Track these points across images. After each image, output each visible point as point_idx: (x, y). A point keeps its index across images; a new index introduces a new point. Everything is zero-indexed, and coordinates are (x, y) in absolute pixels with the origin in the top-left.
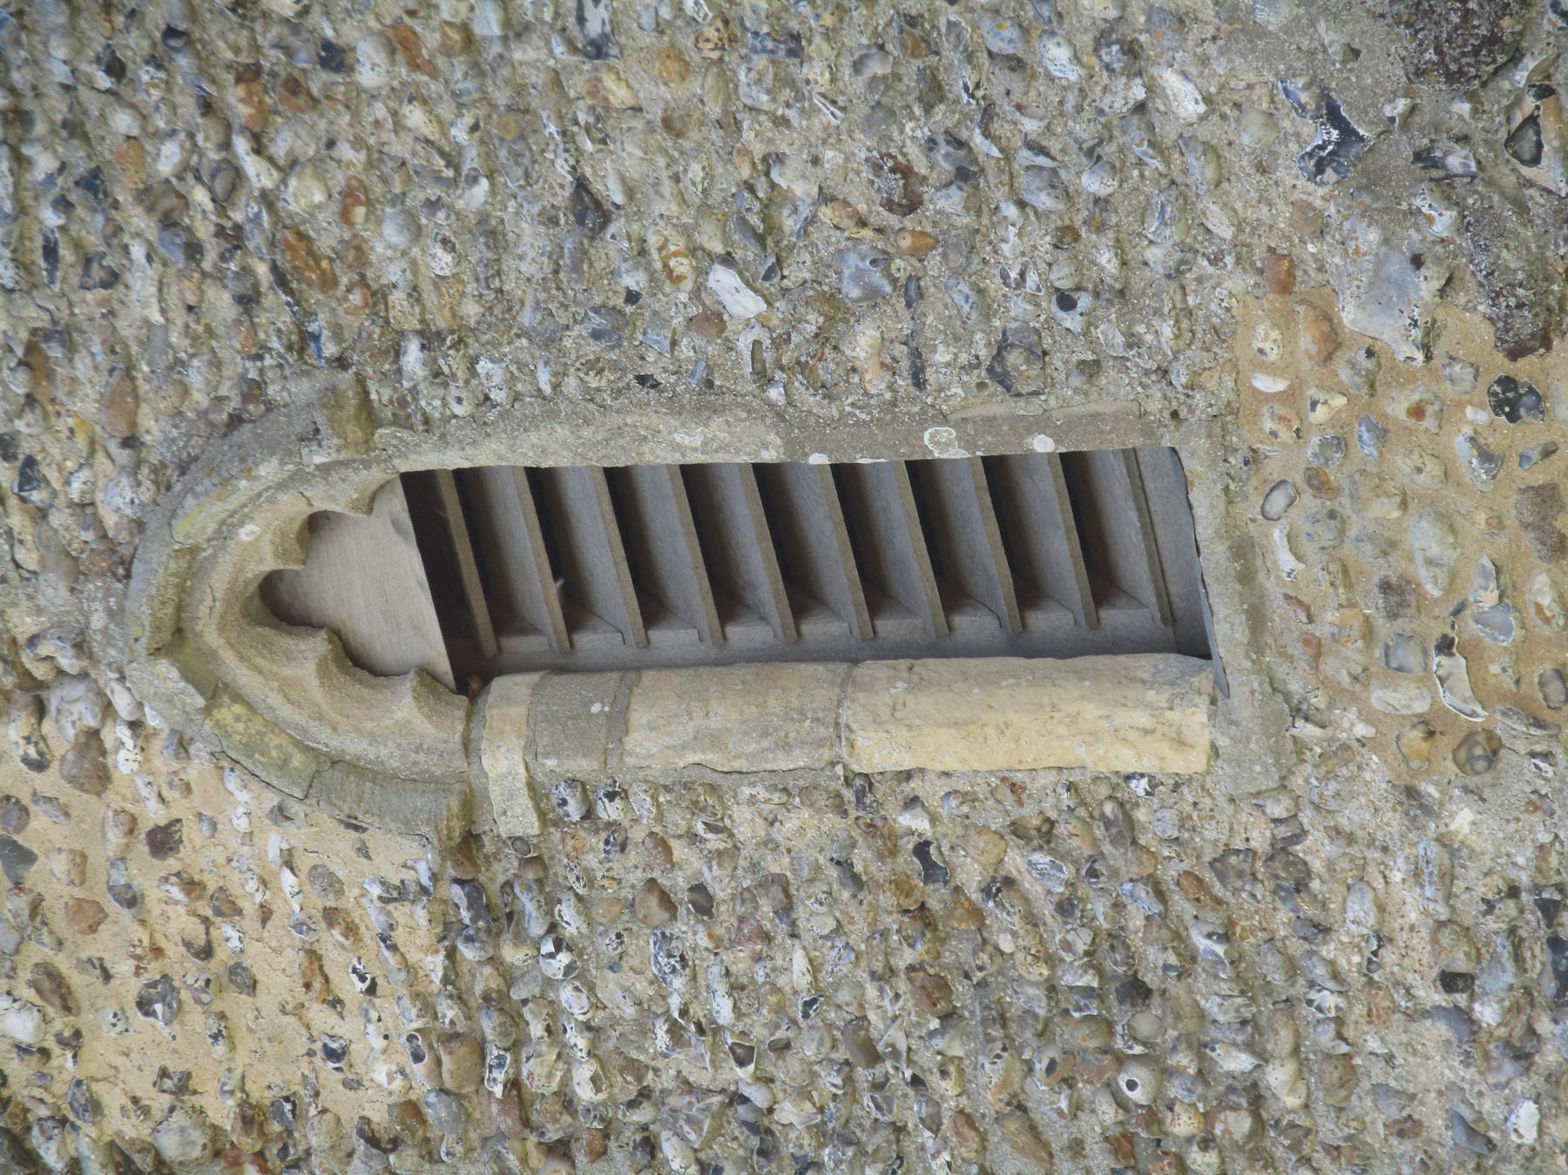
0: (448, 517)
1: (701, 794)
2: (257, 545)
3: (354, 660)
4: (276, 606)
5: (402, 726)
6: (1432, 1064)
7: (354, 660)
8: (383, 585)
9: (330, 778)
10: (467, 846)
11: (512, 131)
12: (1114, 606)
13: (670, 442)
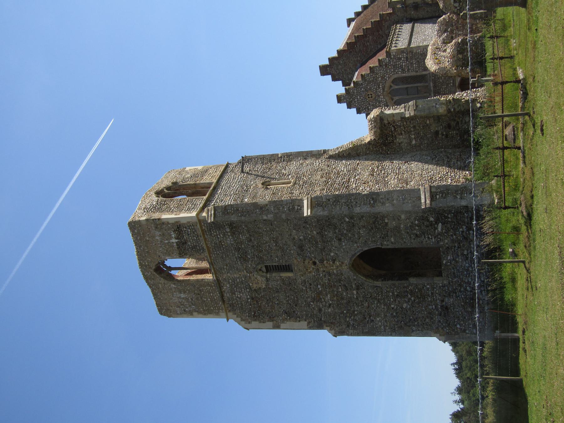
0: (266, 267)
1: (275, 277)
2: (259, 268)
3: (263, 272)
4: (260, 270)
5: (265, 274)
6: (301, 286)
7: (263, 272)
8: (264, 269)
9: (262, 276)
10: (267, 278)
11: (269, 253)
12: (514, 304)
13: (275, 264)
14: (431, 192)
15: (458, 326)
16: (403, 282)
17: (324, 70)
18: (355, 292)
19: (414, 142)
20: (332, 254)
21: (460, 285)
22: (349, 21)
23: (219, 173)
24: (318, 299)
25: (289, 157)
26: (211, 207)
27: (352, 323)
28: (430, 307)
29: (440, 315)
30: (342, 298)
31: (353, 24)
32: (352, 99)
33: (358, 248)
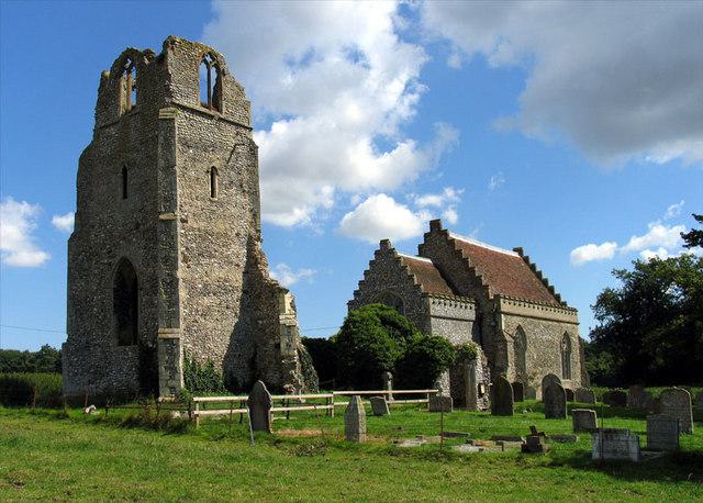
19: (260, 322)
31: (516, 255)
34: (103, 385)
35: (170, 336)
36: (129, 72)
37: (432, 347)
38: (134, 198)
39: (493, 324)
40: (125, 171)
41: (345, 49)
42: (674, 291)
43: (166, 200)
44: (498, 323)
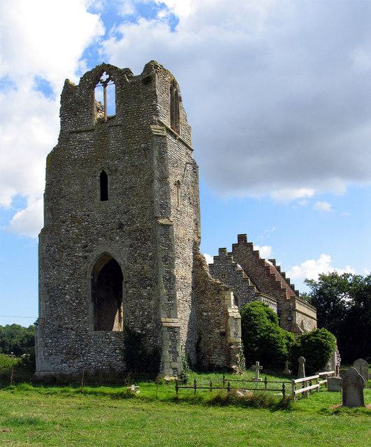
14: (175, 327)
15: (50, 341)
16: (90, 298)
17: (242, 238)
18: (81, 254)
19: (205, 314)
20: (117, 238)
21: (86, 346)
22: (273, 261)
23: (185, 141)
24: (74, 219)
25: (196, 206)
26: (165, 133)
27: (52, 249)
28: (66, 319)
29: (60, 326)
30: (75, 243)
31: (271, 264)
32: (222, 256)
33: (122, 260)
34: (78, 364)
35: (173, 325)
36: (105, 84)
37: (324, 338)
38: (114, 201)
39: (289, 319)
40: (104, 178)
41: (37, 79)
42: (347, 299)
43: (162, 207)
44: (293, 318)
